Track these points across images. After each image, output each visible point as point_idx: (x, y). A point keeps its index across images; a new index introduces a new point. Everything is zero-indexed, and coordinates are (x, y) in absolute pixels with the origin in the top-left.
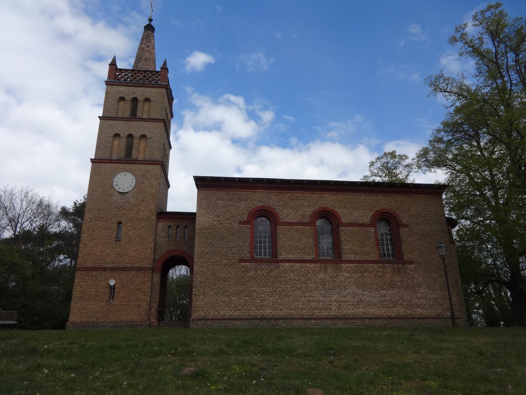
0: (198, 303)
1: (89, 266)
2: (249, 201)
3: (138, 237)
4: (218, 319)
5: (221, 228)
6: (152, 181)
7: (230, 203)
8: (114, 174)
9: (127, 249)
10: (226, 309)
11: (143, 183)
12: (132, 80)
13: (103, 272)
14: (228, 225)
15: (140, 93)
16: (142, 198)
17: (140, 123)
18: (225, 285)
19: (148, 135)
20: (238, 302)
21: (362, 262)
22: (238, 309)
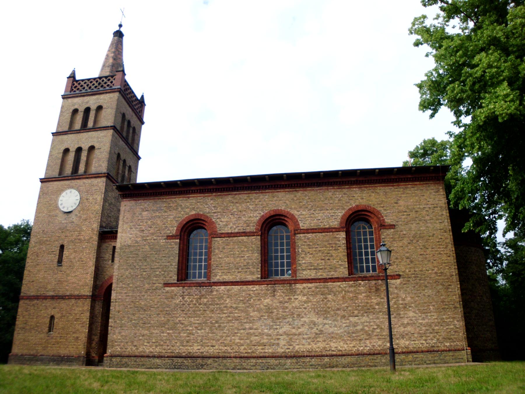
0: (115, 336)
1: (32, 294)
2: (180, 209)
3: (79, 261)
4: (135, 356)
6: (96, 196)
7: (157, 214)
8: (60, 192)
9: (68, 275)
10: (145, 344)
11: (87, 199)
13: (44, 301)
14: (153, 241)
18: (145, 315)
19: (97, 146)
21: (325, 280)
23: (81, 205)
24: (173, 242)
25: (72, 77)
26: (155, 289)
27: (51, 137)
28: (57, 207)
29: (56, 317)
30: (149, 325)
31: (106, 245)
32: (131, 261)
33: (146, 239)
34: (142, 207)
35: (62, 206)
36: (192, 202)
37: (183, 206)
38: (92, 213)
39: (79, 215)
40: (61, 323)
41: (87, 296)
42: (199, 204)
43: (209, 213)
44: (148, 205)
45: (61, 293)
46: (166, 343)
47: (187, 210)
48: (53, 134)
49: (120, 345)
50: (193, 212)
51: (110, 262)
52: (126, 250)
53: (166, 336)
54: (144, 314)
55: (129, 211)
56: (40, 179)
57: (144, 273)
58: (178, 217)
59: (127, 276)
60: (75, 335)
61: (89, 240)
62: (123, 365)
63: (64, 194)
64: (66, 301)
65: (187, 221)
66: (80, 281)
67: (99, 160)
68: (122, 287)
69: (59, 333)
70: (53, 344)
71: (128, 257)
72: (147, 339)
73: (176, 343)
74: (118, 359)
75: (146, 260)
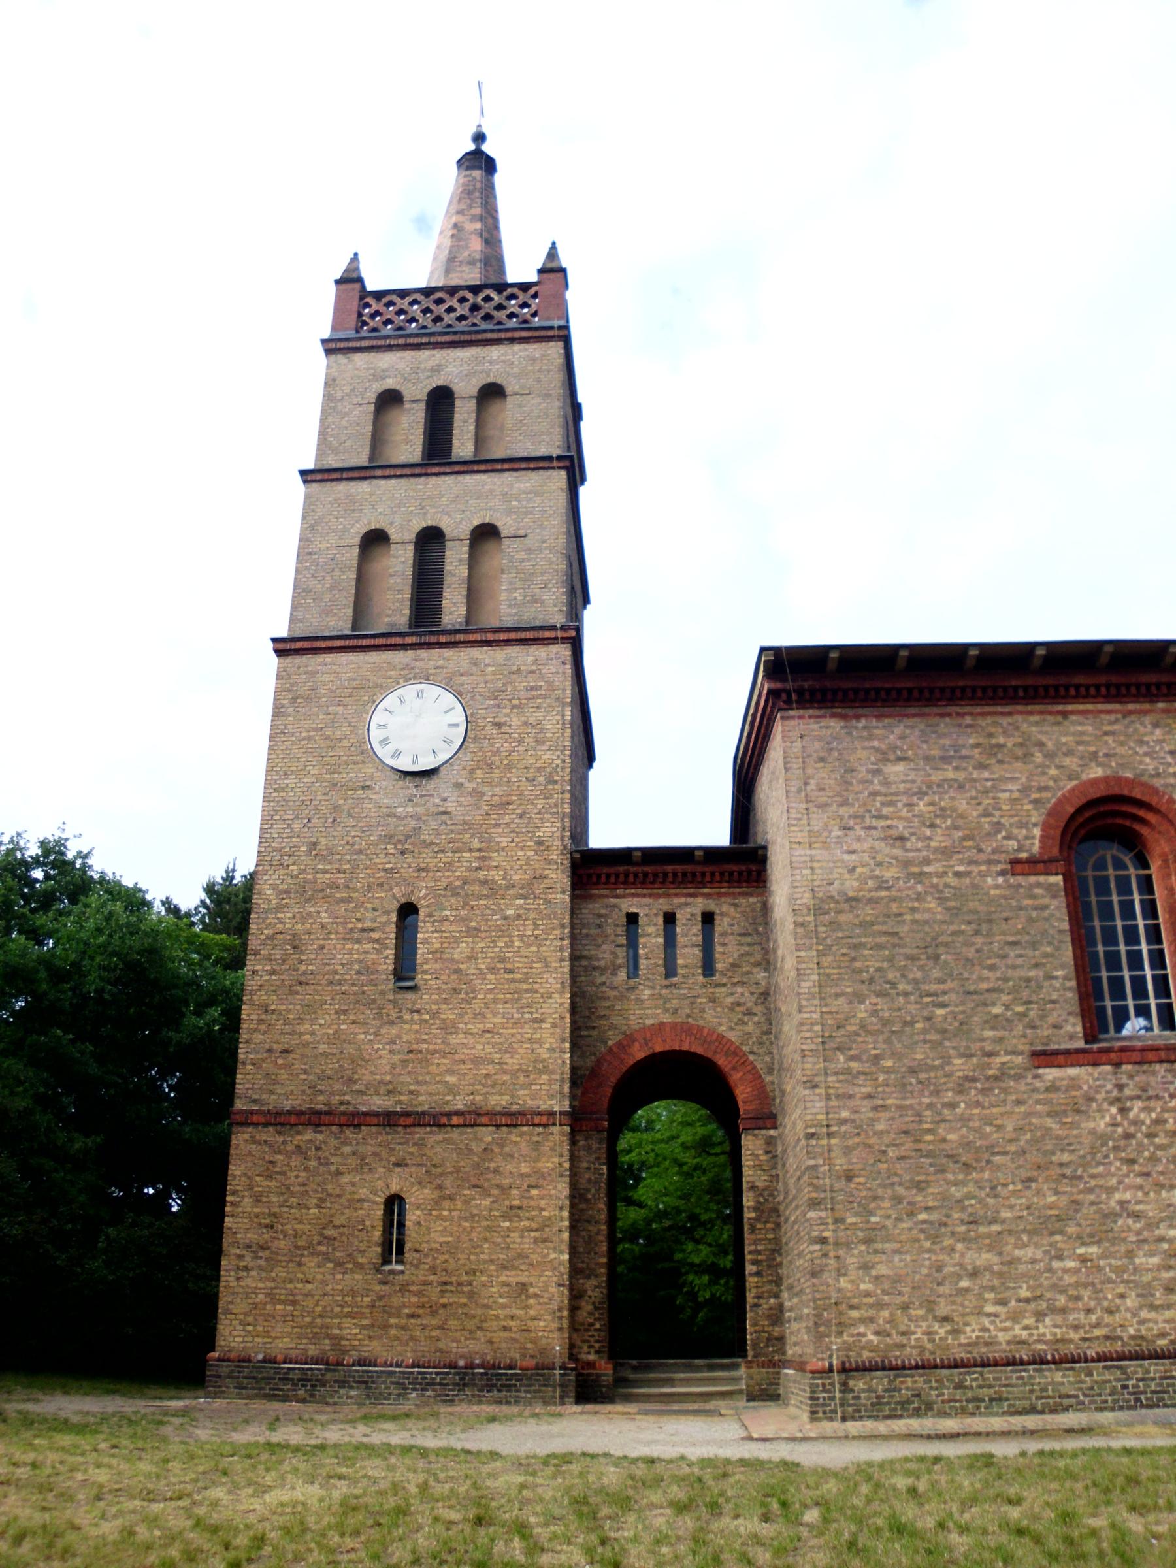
0: (843, 1283)
1: (287, 1105)
2: (1039, 758)
3: (492, 970)
4: (956, 1365)
5: (919, 898)
6: (540, 715)
7: (951, 775)
8: (369, 694)
9: (448, 1028)
10: (989, 1308)
11: (499, 725)
12: (429, 323)
13: (348, 1132)
14: (951, 880)
15: (462, 369)
16: (498, 790)
17: (468, 479)
18: (971, 1188)
19: (506, 525)
20: (1050, 1270)
22: (1054, 1310)
23: (472, 747)
24: (1039, 885)
25: (350, 279)
26: (996, 1078)
27: (299, 488)
28: (366, 753)
29: (409, 1200)
30: (996, 1228)
31: (596, 906)
32: (871, 962)
33: (921, 874)
34: (876, 743)
35: (391, 748)
36: (1082, 733)
37: (1050, 745)
38: (531, 781)
39: (470, 786)
40: (438, 1226)
41: (551, 1114)
42: (1110, 739)
43: (1158, 775)
44: (902, 737)
45: (424, 1103)
46: (1078, 1298)
47: (1070, 762)
48: (307, 476)
49: (871, 1320)
50: (1096, 772)
51: (622, 975)
52: (843, 918)
53: (1076, 1271)
54: (963, 1183)
55: (822, 759)
56: (275, 640)
57: (940, 1012)
58: (1041, 789)
59: (863, 1027)
60: (513, 1277)
61: (529, 885)
62: (904, 1404)
63: (391, 701)
64: (455, 1134)
65: (1078, 803)
66: (511, 1051)
67: (528, 579)
68: (847, 1072)
69: (433, 1270)
70: (412, 1316)
71: (855, 947)
72: (993, 1289)
73: (1122, 1296)
74: (879, 1382)
75: (937, 957)
